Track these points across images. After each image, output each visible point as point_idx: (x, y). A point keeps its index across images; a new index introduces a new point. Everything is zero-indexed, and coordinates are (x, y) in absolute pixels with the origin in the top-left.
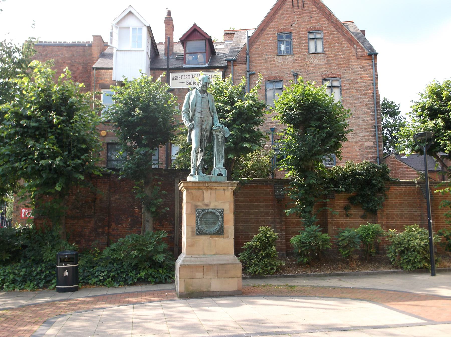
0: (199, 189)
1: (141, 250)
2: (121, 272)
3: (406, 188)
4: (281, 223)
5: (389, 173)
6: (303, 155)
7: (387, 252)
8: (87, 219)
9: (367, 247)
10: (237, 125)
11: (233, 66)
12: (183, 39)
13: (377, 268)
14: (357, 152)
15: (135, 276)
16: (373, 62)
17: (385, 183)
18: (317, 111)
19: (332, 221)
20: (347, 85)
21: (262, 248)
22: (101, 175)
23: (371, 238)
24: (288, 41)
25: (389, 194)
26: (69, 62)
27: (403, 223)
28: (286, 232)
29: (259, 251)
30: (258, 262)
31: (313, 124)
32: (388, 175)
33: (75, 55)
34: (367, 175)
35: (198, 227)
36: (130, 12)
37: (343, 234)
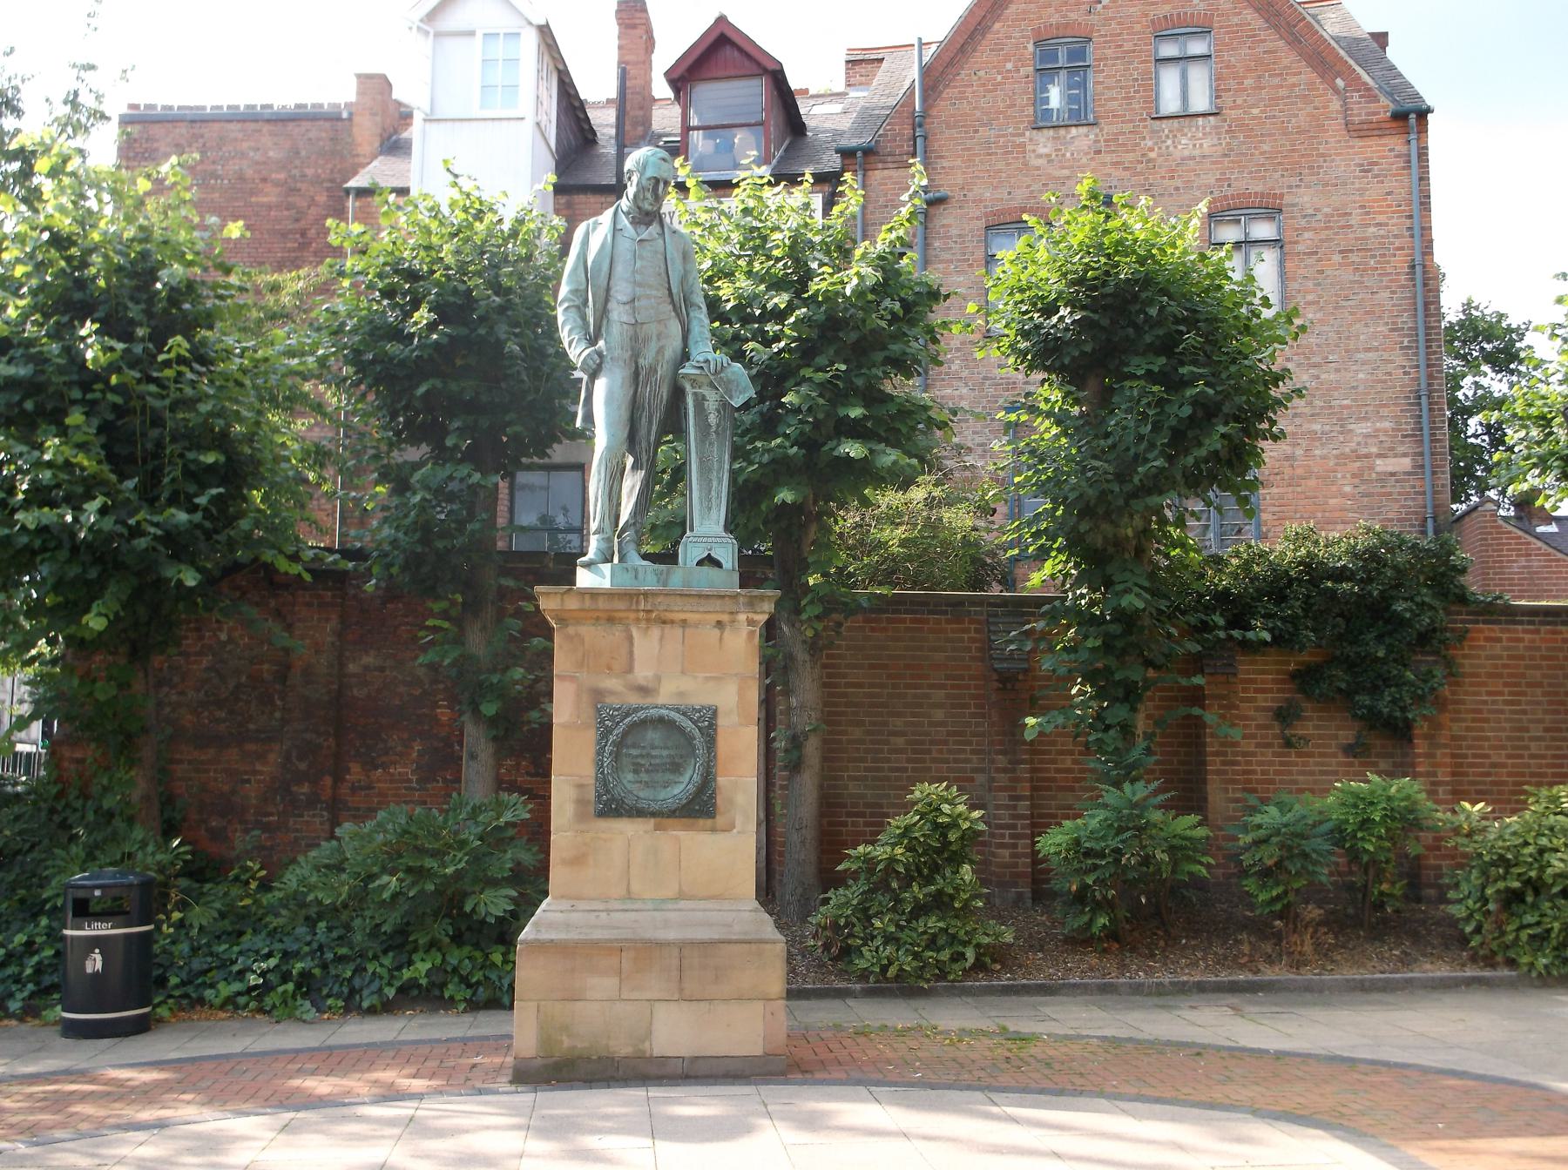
0: (611, 620)
1: (418, 873)
2: (340, 959)
3: (1537, 632)
4: (1014, 771)
5: (1463, 571)
6: (1090, 492)
7: (1451, 895)
8: (251, 747)
9: (1366, 872)
10: (819, 370)
11: (865, 170)
12: (675, 76)
13: (1406, 961)
14: (1344, 496)
15: (392, 977)
16: (1414, 143)
17: (1448, 613)
18: (1153, 312)
19: (1224, 763)
20: (1306, 235)
21: (919, 871)
22: (307, 577)
23: (1380, 838)
24: (1078, 69)
25: (1465, 656)
26: (282, 176)
27: (1523, 775)
28: (1033, 806)
29: (907, 882)
30: (902, 928)
31: (1138, 365)
32: (1462, 579)
33: (303, 153)
34: (1370, 580)
35: (603, 782)
37: (1258, 819)
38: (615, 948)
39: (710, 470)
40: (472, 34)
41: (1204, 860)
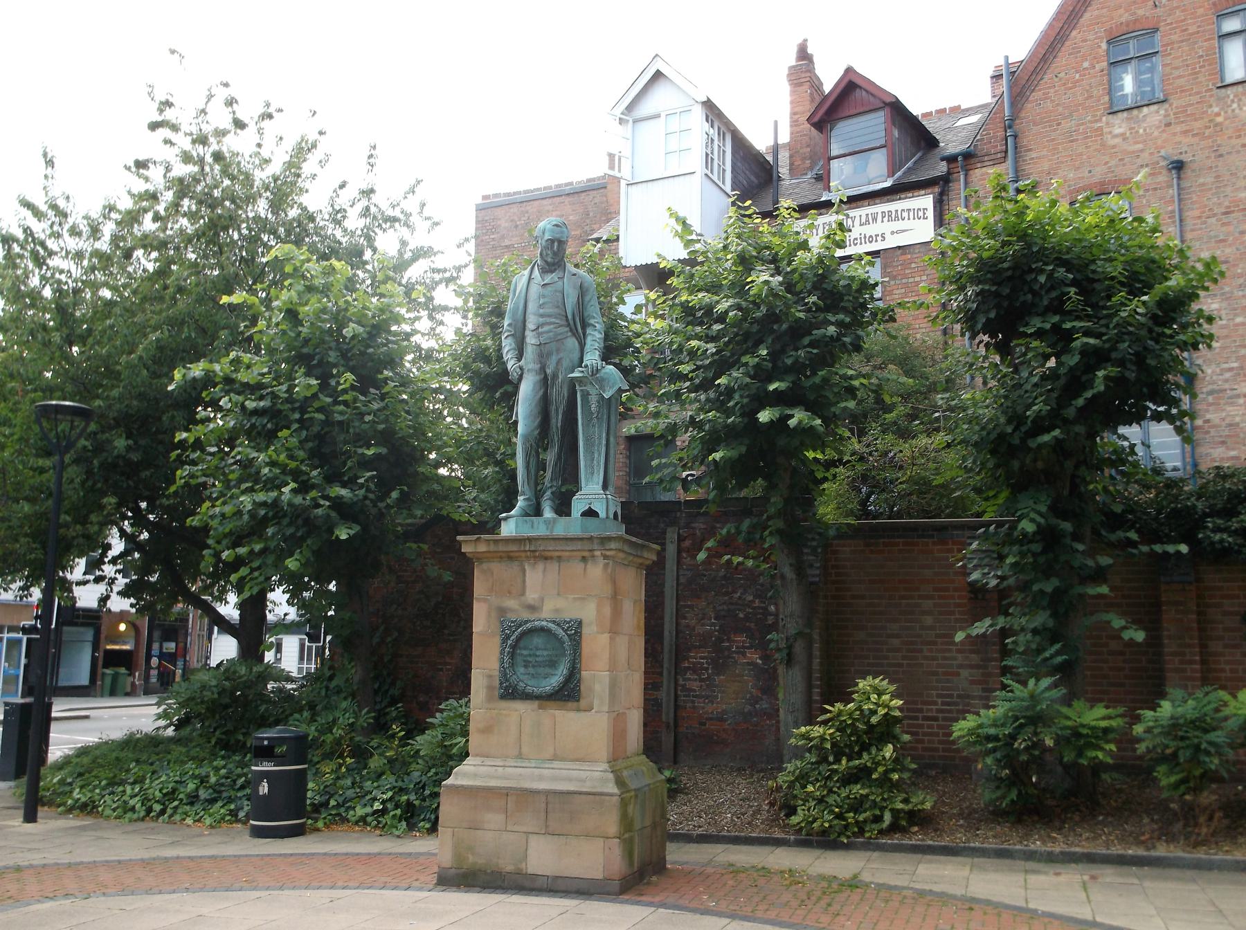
12: (816, 119)
26: (578, 232)
35: (504, 675)
36: (658, 75)
38: (505, 793)
39: (593, 445)
40: (658, 116)
41: (1107, 747)
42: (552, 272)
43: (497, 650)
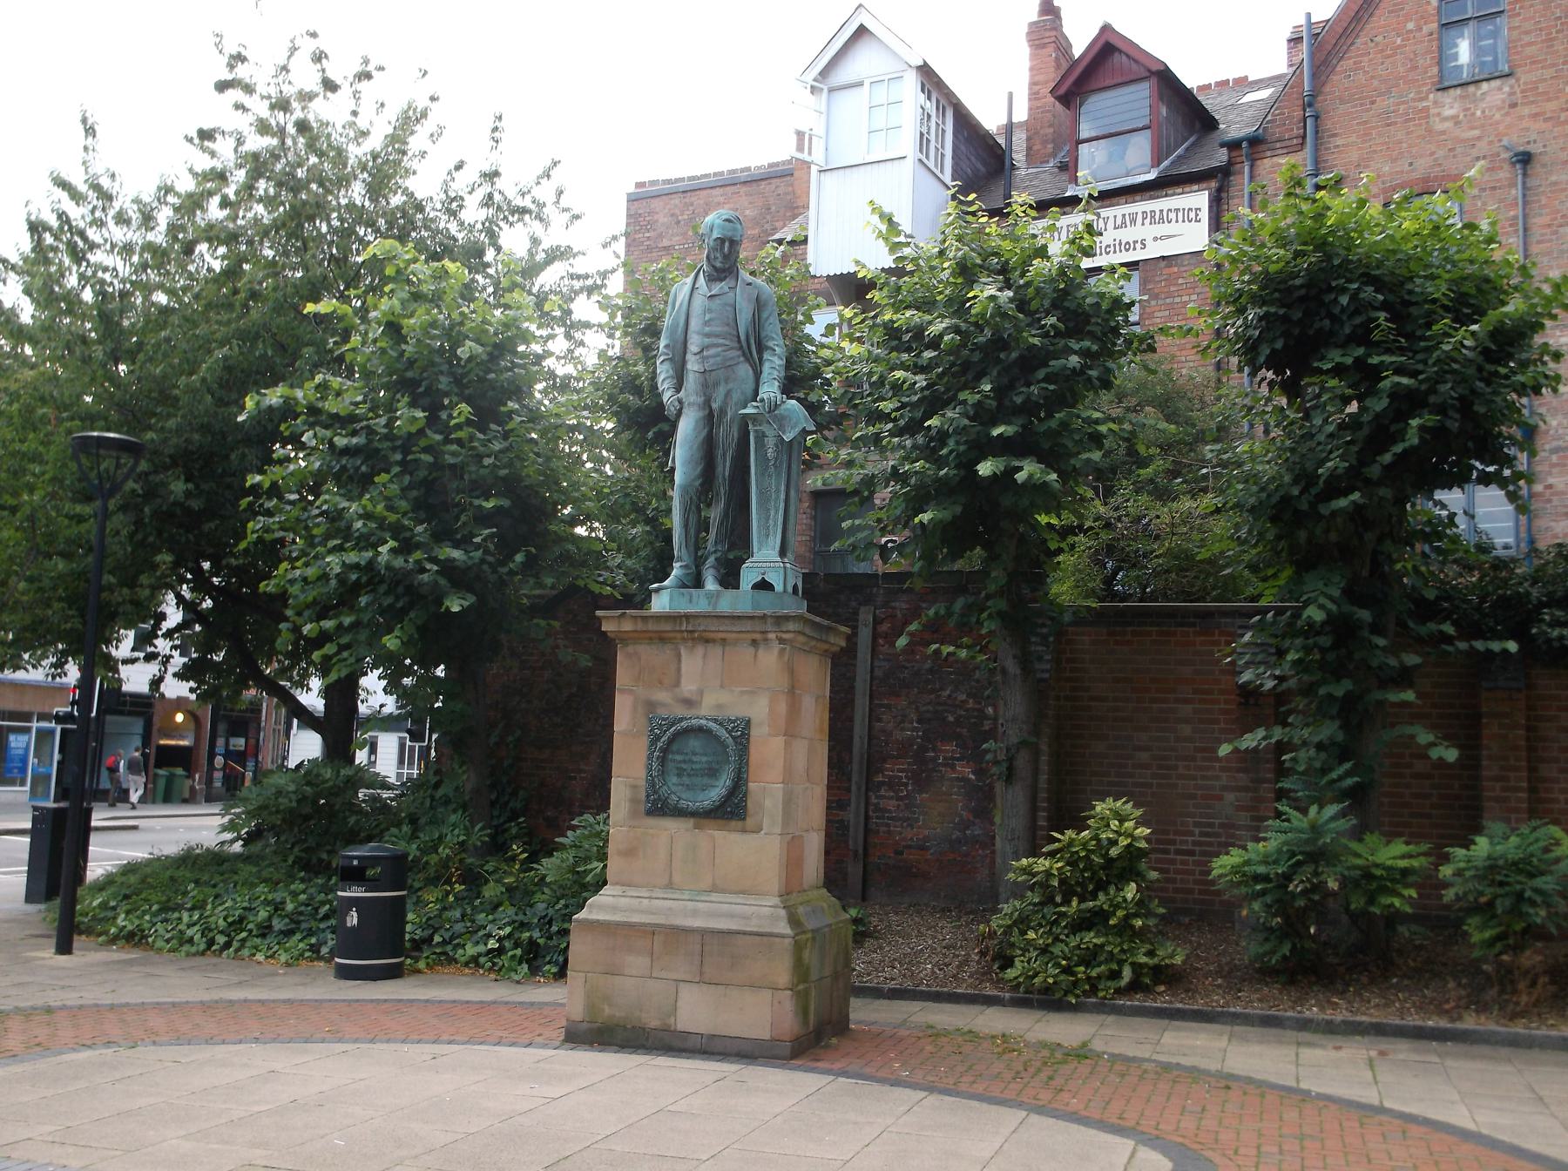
12: (1062, 91)
36: (862, 31)
38: (650, 931)
42: (721, 280)
43: (644, 753)
